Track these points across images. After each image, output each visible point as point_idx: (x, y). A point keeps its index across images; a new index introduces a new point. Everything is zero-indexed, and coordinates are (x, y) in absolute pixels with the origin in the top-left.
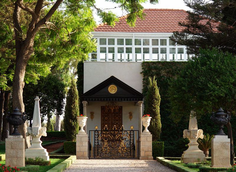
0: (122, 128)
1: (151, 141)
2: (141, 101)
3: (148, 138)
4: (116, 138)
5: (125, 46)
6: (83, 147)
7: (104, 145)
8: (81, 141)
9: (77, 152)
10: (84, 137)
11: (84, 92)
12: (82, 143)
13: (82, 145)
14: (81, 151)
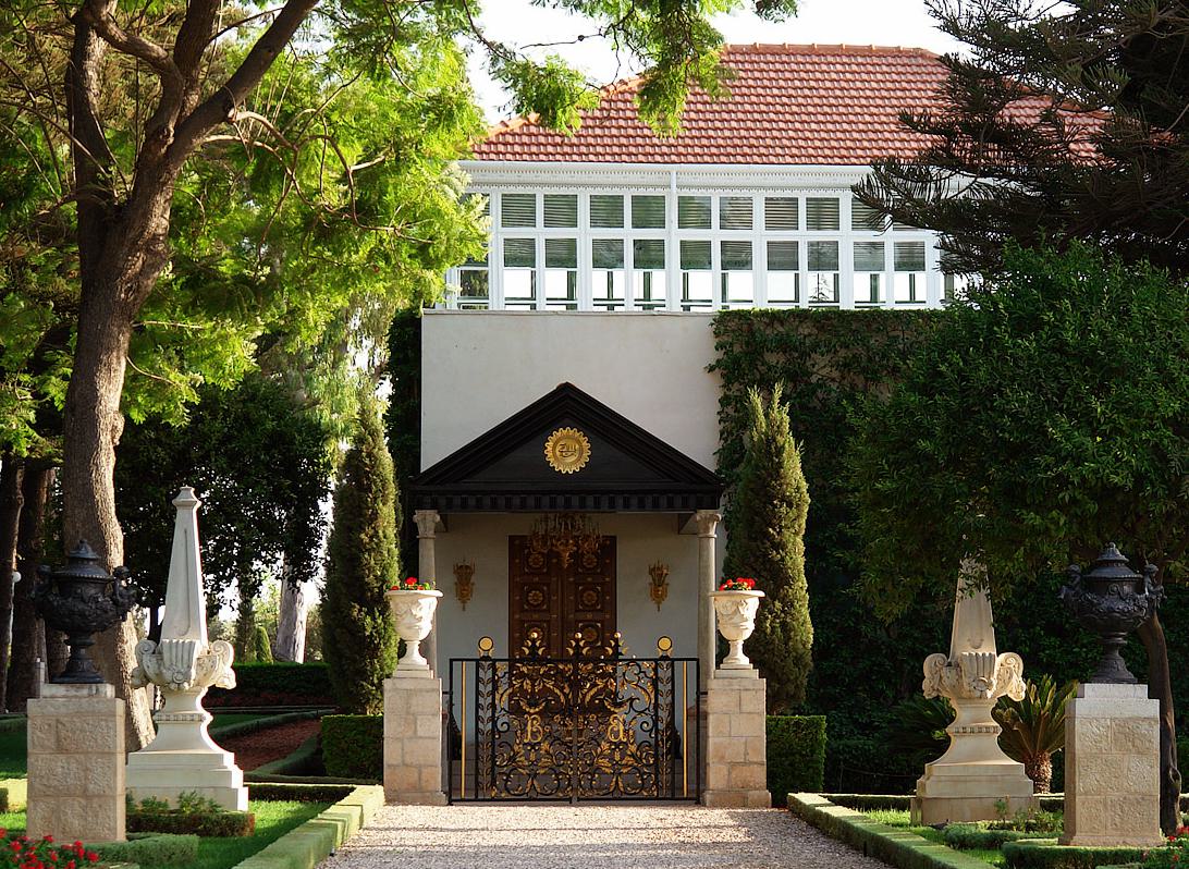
0: (617, 645)
1: (759, 714)
2: (711, 512)
3: (744, 694)
4: (584, 696)
5: (628, 234)
6: (421, 741)
7: (524, 731)
8: (408, 713)
9: (389, 766)
10: (421, 691)
11: (425, 466)
12: (415, 723)
13: (415, 731)
14: (407, 765)
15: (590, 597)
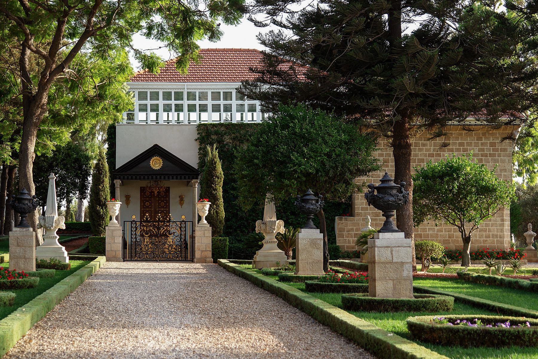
7: (144, 241)
15: (162, 204)
